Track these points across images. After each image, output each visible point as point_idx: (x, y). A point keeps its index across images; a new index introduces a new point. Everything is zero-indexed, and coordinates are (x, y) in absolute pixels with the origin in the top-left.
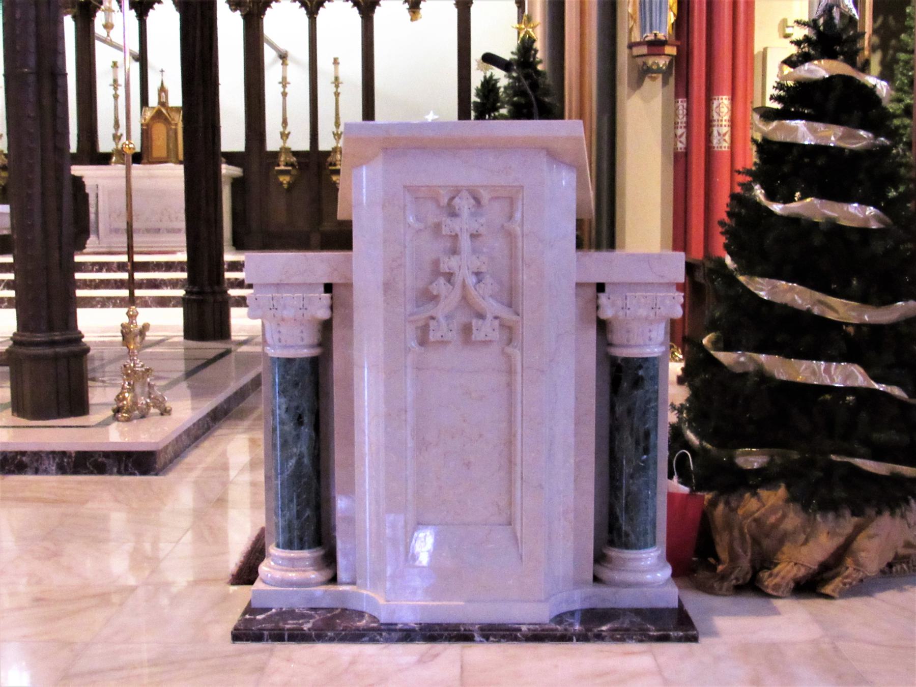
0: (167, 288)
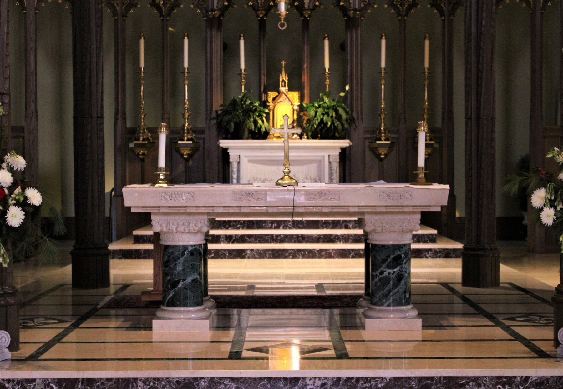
0: (340, 243)
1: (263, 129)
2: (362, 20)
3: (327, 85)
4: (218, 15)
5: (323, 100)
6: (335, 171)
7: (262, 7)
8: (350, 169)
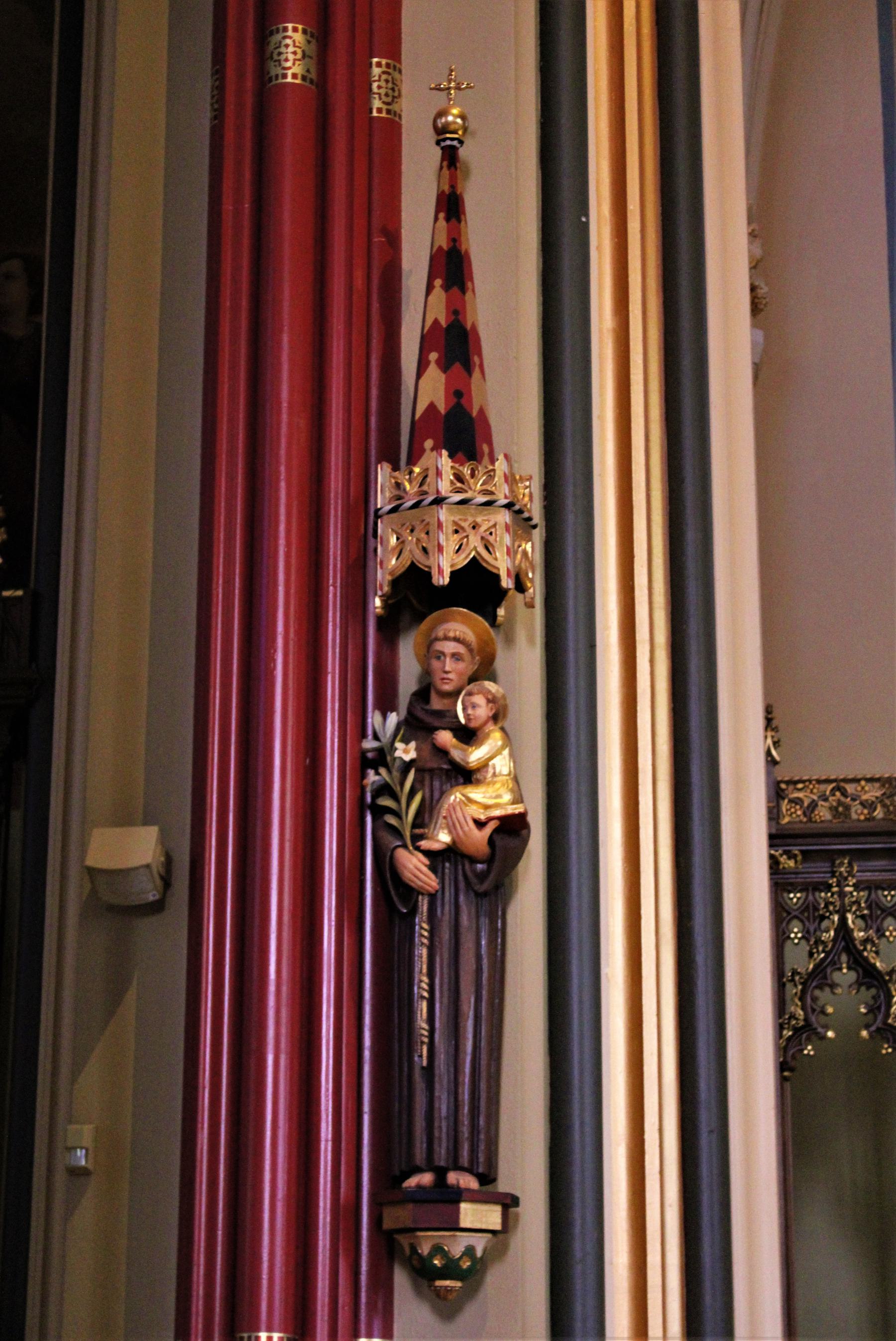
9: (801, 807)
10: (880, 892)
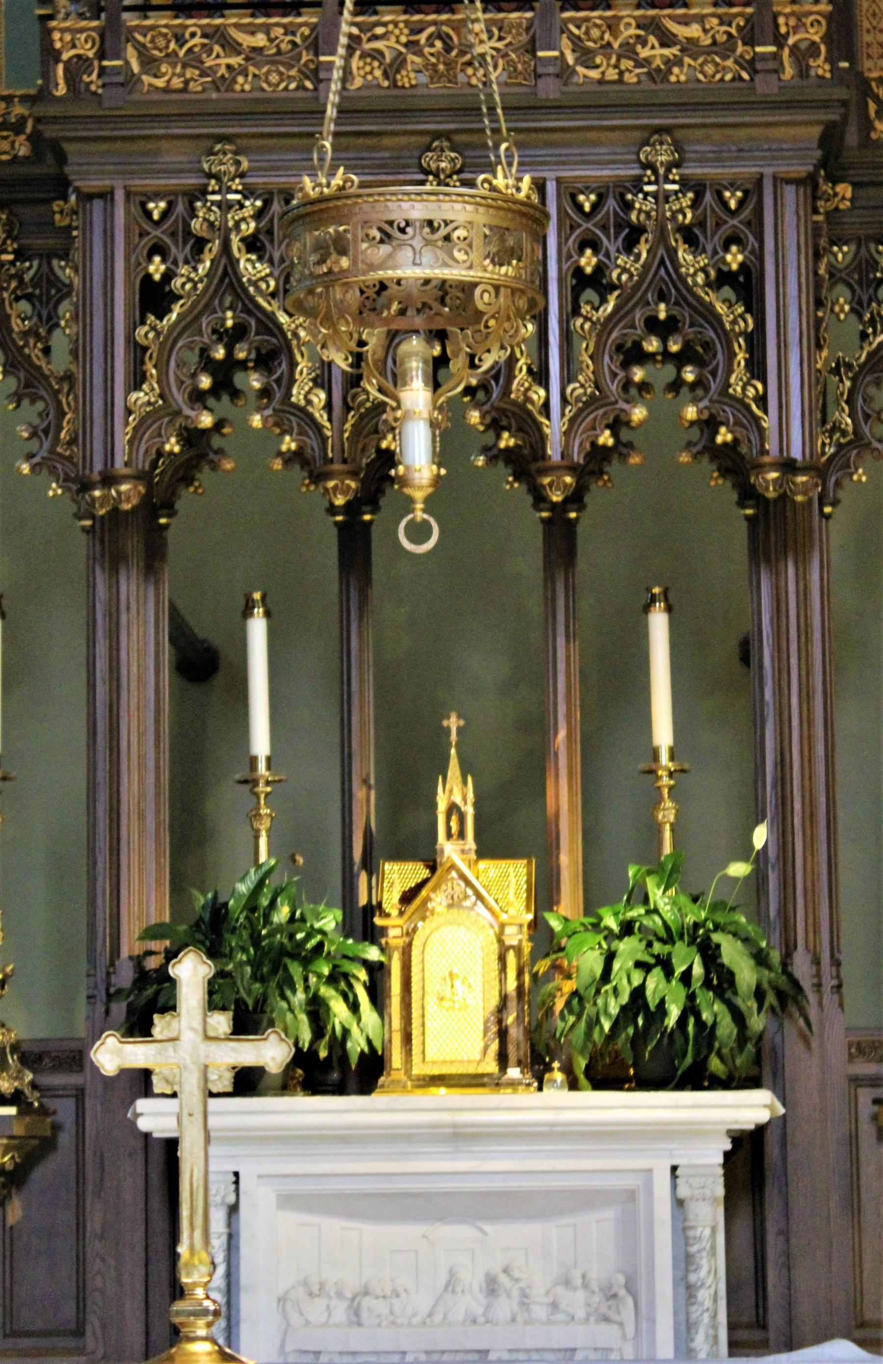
1: (357, 1045)
2: (828, 517)
3: (668, 827)
4: (135, 501)
5: (646, 900)
6: (706, 1244)
7: (345, 461)
8: (785, 1233)
9: (381, 64)
10: (55, 262)
